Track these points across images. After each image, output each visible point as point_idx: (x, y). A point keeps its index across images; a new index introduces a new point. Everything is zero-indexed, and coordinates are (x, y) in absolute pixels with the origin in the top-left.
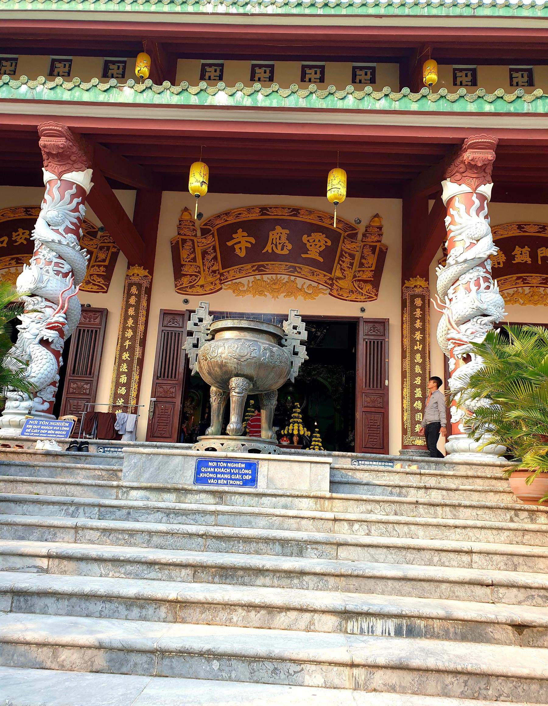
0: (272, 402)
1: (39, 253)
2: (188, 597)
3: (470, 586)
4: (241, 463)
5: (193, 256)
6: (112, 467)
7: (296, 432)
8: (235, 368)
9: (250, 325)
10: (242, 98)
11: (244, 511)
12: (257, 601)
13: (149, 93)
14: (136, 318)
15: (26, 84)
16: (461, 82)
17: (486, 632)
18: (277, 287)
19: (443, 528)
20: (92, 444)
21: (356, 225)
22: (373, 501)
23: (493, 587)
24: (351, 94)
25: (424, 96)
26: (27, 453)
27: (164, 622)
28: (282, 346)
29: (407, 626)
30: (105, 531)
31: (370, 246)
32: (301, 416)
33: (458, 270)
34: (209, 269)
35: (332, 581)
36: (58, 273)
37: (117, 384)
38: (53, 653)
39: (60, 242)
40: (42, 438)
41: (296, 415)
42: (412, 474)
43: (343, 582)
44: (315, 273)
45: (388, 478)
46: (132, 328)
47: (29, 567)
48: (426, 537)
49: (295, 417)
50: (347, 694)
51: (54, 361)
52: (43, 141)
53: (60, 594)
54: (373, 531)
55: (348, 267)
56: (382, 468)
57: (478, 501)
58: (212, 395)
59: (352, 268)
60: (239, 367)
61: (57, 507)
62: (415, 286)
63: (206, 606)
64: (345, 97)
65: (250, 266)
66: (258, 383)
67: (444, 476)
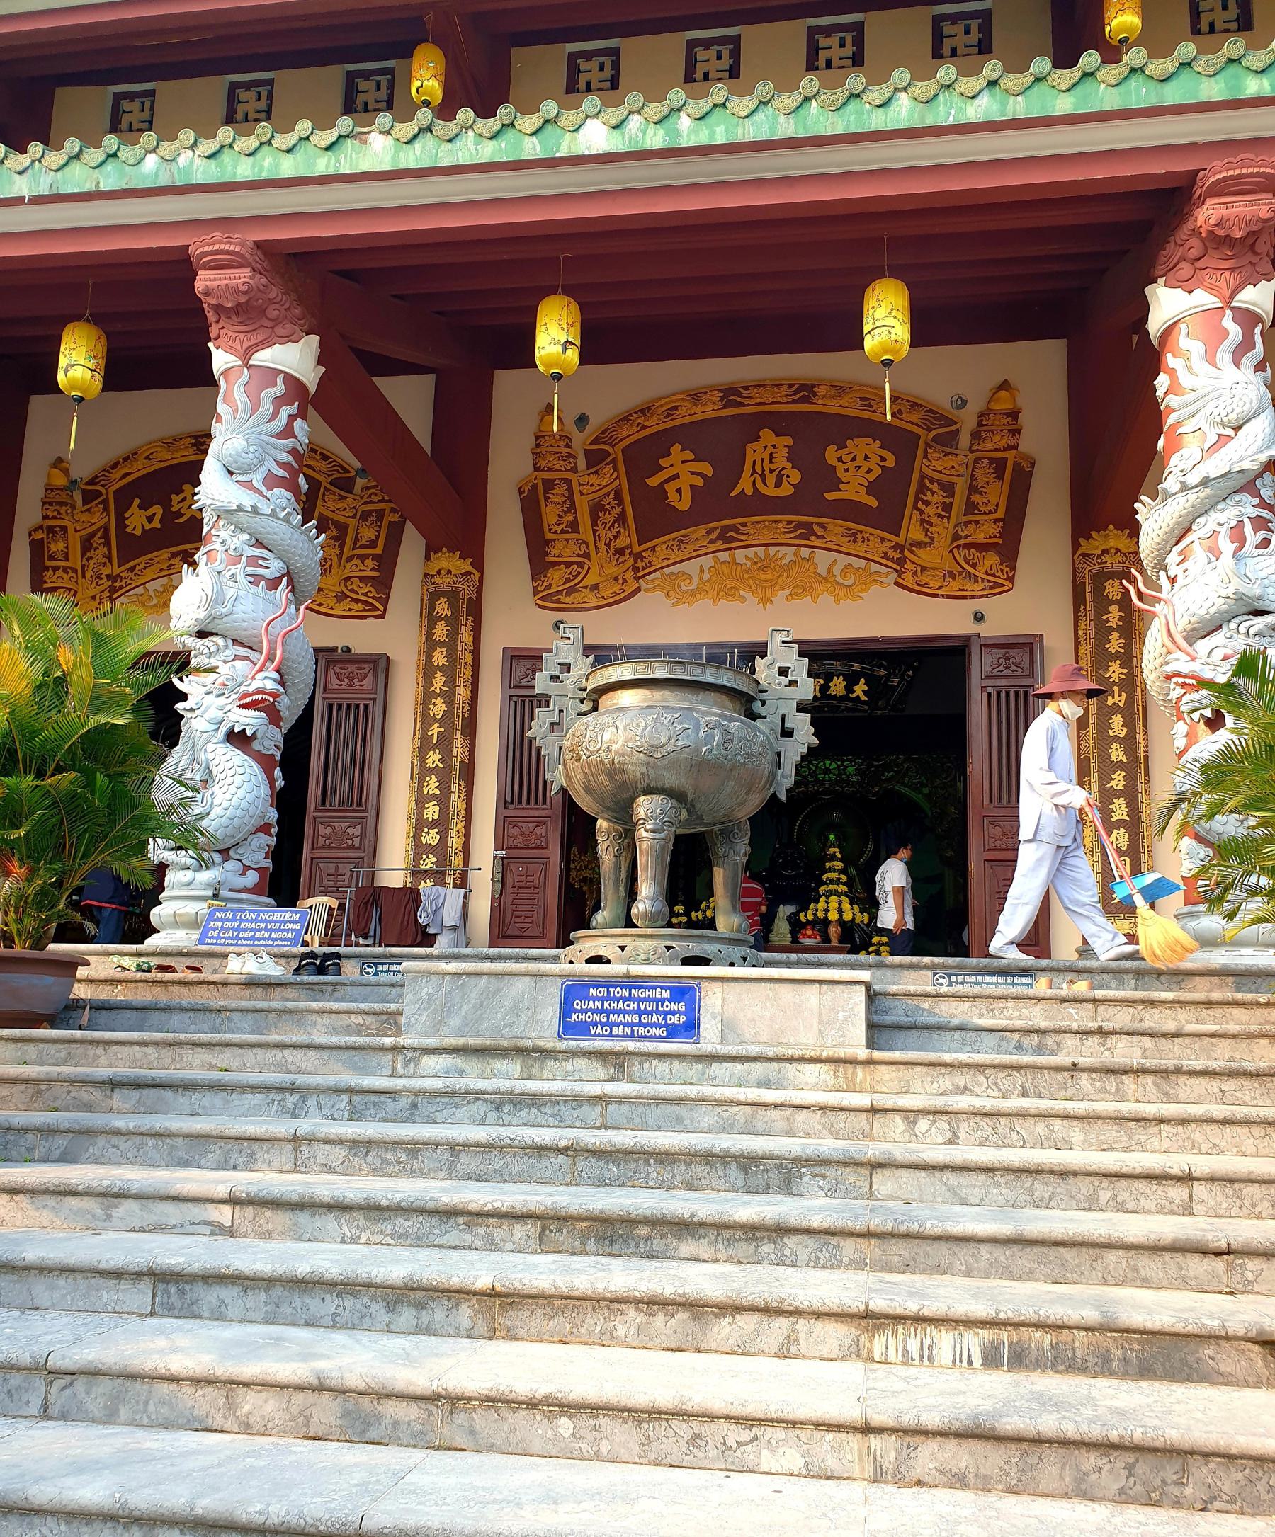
0: (737, 848)
1: (214, 539)
2: (517, 1284)
3: (1175, 1255)
4: (662, 988)
5: (570, 517)
6: (387, 1005)
7: (833, 916)
8: (642, 774)
9: (674, 672)
10: (643, 132)
11: (664, 1095)
12: (668, 1292)
13: (428, 141)
14: (450, 673)
15: (154, 150)
16: (1212, 25)
17: (1200, 1359)
18: (769, 577)
19: (1131, 1124)
20: (348, 957)
21: (956, 412)
22: (968, 1066)
23: (1232, 1256)
24: (905, 89)
25: (1088, 75)
26: (209, 983)
27: (468, 1337)
28: (753, 716)
29: (1010, 1345)
30: (356, 1144)
31: (991, 461)
32: (844, 878)
33: (1189, 504)
34: (608, 545)
35: (849, 1247)
36: (256, 580)
37: (420, 824)
38: (227, 1398)
39: (255, 510)
40: (242, 949)
41: (834, 875)
42: (1075, 1001)
43: (874, 1249)
44: (860, 536)
45: (1016, 1014)
46: (442, 694)
47: (194, 1224)
48: (1091, 1144)
49: (831, 882)
50: (856, 1490)
51: (261, 777)
52: (204, 281)
53: (247, 1278)
54: (962, 1135)
55: (940, 516)
56: (1001, 990)
57: (1231, 1059)
58: (600, 839)
59: (948, 518)
60: (651, 771)
61: (261, 1096)
62: (1105, 551)
63: (557, 1302)
64: (890, 99)
65: (704, 532)
66: (698, 806)
67: (1153, 1003)
